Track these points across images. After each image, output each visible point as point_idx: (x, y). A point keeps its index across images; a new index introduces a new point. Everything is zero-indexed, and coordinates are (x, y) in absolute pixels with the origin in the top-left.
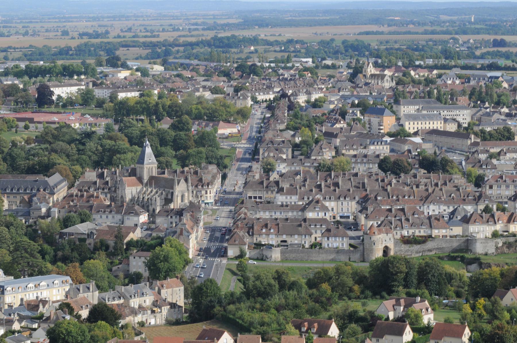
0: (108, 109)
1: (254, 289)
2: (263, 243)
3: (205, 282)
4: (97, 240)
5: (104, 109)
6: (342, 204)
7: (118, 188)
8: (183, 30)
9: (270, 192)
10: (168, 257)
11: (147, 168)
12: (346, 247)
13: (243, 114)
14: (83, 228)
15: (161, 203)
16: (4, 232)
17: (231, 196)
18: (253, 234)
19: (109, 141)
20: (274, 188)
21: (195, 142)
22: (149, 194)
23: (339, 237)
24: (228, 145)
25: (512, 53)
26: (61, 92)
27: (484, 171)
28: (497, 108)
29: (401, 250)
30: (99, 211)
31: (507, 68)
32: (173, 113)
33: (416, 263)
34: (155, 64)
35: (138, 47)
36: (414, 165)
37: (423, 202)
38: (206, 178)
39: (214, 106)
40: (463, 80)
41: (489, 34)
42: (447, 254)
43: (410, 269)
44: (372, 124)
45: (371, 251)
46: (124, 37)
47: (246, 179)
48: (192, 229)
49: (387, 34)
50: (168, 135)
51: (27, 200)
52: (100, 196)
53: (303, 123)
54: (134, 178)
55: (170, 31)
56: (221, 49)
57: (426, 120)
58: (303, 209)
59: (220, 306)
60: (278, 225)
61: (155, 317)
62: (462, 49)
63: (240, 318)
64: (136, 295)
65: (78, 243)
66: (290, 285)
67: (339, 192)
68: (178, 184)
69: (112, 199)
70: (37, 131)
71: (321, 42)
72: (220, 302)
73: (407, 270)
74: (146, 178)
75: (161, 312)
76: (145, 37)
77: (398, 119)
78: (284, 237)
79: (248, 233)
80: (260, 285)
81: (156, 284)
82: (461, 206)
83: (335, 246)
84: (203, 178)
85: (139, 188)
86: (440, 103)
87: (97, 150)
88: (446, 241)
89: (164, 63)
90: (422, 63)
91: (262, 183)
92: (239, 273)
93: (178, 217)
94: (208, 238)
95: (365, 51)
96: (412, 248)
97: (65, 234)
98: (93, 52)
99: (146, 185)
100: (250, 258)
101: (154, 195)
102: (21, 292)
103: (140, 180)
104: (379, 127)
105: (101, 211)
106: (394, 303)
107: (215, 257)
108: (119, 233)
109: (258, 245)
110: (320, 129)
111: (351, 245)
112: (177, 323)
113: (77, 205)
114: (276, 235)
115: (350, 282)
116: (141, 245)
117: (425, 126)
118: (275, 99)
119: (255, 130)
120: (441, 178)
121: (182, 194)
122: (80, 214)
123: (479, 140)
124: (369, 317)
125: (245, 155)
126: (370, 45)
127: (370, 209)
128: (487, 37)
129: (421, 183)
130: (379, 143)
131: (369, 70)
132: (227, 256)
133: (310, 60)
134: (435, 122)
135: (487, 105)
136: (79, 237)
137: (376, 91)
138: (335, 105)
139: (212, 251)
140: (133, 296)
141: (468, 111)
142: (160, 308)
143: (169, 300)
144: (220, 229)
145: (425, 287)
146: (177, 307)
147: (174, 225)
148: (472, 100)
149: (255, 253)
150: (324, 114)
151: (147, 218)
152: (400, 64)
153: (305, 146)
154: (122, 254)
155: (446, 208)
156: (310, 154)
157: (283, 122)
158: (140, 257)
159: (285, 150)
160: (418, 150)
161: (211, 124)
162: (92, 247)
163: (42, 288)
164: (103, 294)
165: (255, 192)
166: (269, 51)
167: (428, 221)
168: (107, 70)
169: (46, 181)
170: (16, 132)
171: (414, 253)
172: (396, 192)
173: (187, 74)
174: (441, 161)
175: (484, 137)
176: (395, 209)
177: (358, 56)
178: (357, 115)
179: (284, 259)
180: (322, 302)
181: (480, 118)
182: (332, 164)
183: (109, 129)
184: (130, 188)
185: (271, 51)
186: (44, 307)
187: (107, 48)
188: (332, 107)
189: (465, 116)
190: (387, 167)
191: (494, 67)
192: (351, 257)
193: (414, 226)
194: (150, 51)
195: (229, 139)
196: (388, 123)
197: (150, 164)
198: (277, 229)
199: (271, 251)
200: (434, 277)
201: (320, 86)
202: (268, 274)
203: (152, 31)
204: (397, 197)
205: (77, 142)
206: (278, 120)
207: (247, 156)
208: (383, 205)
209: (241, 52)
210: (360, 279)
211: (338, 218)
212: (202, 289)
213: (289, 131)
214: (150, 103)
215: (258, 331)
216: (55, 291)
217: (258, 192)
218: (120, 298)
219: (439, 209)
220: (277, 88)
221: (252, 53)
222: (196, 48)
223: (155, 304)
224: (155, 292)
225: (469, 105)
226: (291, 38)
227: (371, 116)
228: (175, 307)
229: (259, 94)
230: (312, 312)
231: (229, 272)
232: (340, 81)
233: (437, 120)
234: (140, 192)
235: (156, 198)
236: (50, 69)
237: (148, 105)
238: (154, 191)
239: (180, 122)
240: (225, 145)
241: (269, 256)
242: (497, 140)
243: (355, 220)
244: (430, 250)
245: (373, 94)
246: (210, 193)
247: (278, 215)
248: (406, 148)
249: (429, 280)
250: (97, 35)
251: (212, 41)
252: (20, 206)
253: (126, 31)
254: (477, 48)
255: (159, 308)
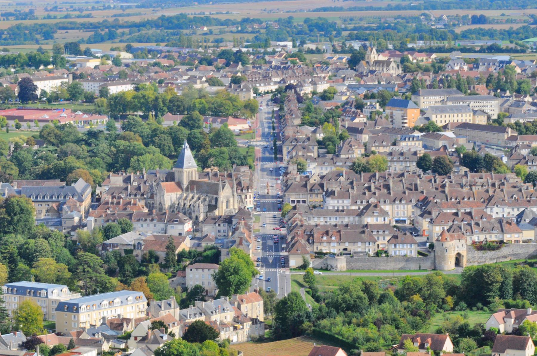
0: (100, 105)
1: (343, 302)
2: (325, 252)
3: (289, 295)
4: (145, 252)
5: (95, 105)
6: (398, 208)
7: (156, 194)
8: (114, 7)
9: (314, 196)
10: (238, 270)
11: (186, 171)
12: (414, 254)
13: (251, 108)
14: (128, 239)
15: (204, 209)
16: (44, 244)
17: (267, 200)
18: (313, 242)
19: (122, 142)
20: (319, 192)
21: (211, 140)
22: (190, 200)
23: (407, 244)
24: (244, 143)
25: (495, 31)
26: (46, 85)
27: (530, 168)
28: (520, 97)
29: (474, 257)
30: (139, 220)
31: (508, 51)
32: (175, 108)
33: (511, 271)
34: (120, 51)
35: (78, 28)
36: (455, 163)
37: (485, 204)
38: (245, 182)
39: (219, 100)
40: (472, 66)
41: (461, 8)
42: (524, 261)
43: (506, 278)
44: (394, 118)
45: (443, 258)
46: (55, 18)
47: (287, 181)
48: (250, 238)
49: (347, 10)
50: (181, 133)
51: (56, 208)
52: (138, 203)
53: (319, 117)
54: (173, 182)
55: (100, 9)
56: (172, 31)
57: (454, 112)
58: (361, 214)
59: (310, 321)
60: (339, 231)
61: (237, 333)
62: (439, 26)
63: (339, 334)
64: (217, 311)
65: (123, 254)
66: (380, 297)
67: (394, 194)
68: (223, 188)
69: (150, 207)
70: (29, 130)
71: (279, 20)
72: (308, 316)
73: (502, 280)
74: (185, 183)
75: (243, 328)
76: (79, 17)
77: (422, 112)
78: (347, 245)
79: (308, 240)
80: (350, 298)
81: (235, 299)
82: (529, 208)
83: (403, 254)
84: (242, 182)
85: (180, 193)
86: (460, 92)
87: (110, 151)
88: (522, 247)
89: (129, 49)
90: (415, 46)
91: (305, 186)
92: (306, 285)
93: (227, 224)
94: (261, 247)
95: (332, 31)
96: (485, 255)
97: (109, 245)
98: (29, 36)
99: (187, 189)
100: (315, 269)
101: (196, 202)
102: (95, 310)
103: (179, 184)
104: (403, 121)
105: (142, 219)
106: (504, 315)
107: (276, 267)
108: (171, 243)
109: (319, 255)
110: (343, 123)
111: (419, 253)
112: (261, 340)
113: (114, 214)
114: (337, 242)
115: (442, 293)
116: (194, 256)
117: (453, 119)
118: (279, 91)
119: (266, 125)
120: (493, 177)
121: (228, 201)
122: (120, 223)
123: (516, 134)
124: (480, 331)
125: (264, 154)
126: (336, 23)
127: (434, 214)
128: (462, 13)
129: (477, 184)
130: (411, 139)
131: (372, 56)
132: (288, 266)
133: (290, 44)
134: (464, 115)
135: (508, 93)
136: (125, 248)
137: (384, 79)
138: (347, 97)
139: (271, 261)
140: (214, 312)
141: (496, 102)
142: (242, 324)
143: (249, 315)
144: (270, 237)
145: (520, 297)
146: (258, 323)
147: (230, 234)
148: (489, 87)
149: (318, 262)
150: (337, 107)
151: (191, 226)
152: (390, 47)
153: (330, 143)
154: (174, 266)
155: (510, 210)
156: (339, 152)
157: (297, 117)
158: (197, 269)
159: (311, 147)
160: (455, 146)
161: (219, 120)
162: (139, 259)
163: (116, 305)
164: (185, 311)
165: (298, 196)
166: (225, 32)
167: (499, 225)
168: (73, 58)
169: (73, 187)
170: (7, 132)
171: (487, 259)
172: (454, 194)
173: (165, 63)
174: (484, 158)
175: (519, 130)
176: (462, 213)
177: (325, 36)
178: (375, 108)
179: (350, 269)
180: (420, 316)
181: (508, 109)
182: (368, 163)
183: (111, 127)
184: (169, 194)
185: (227, 32)
186: (127, 326)
187: (43, 31)
188: (344, 98)
189: (493, 107)
190: (426, 165)
191: (494, 50)
192: (421, 265)
193: (485, 231)
194: (93, 33)
195: (242, 136)
196: (413, 117)
197: (189, 167)
198: (339, 237)
199: (337, 260)
200: (530, 286)
201: (319, 75)
202: (356, 286)
203: (81, 10)
204: (456, 199)
205: (84, 143)
206: (292, 115)
207: (267, 155)
208: (444, 208)
209: (194, 33)
210: (452, 290)
211: (394, 223)
212: (287, 303)
213: (307, 126)
214: (149, 98)
215: (369, 348)
216: (128, 308)
217: (301, 196)
218: (201, 314)
219: (503, 211)
220: (275, 77)
221: (205, 34)
222: (142, 30)
223: (236, 320)
224: (235, 307)
225: (489, 93)
226: (246, 17)
227: (394, 108)
228: (256, 323)
229: (260, 85)
230: (415, 326)
231: (297, 285)
232: (340, 69)
233: (466, 112)
234: (180, 198)
235: (199, 205)
236: (15, 58)
237: (146, 99)
238: (196, 196)
239: (190, 118)
240: (241, 143)
241: (334, 266)
242: (533, 133)
243: (413, 225)
244: (505, 257)
245: (382, 83)
246: (250, 198)
247: (333, 221)
248: (440, 144)
249: (524, 290)
250: (25, 16)
251: (160, 21)
252: (48, 215)
253: (51, 10)
254: (454, 25)
255: (241, 324)
